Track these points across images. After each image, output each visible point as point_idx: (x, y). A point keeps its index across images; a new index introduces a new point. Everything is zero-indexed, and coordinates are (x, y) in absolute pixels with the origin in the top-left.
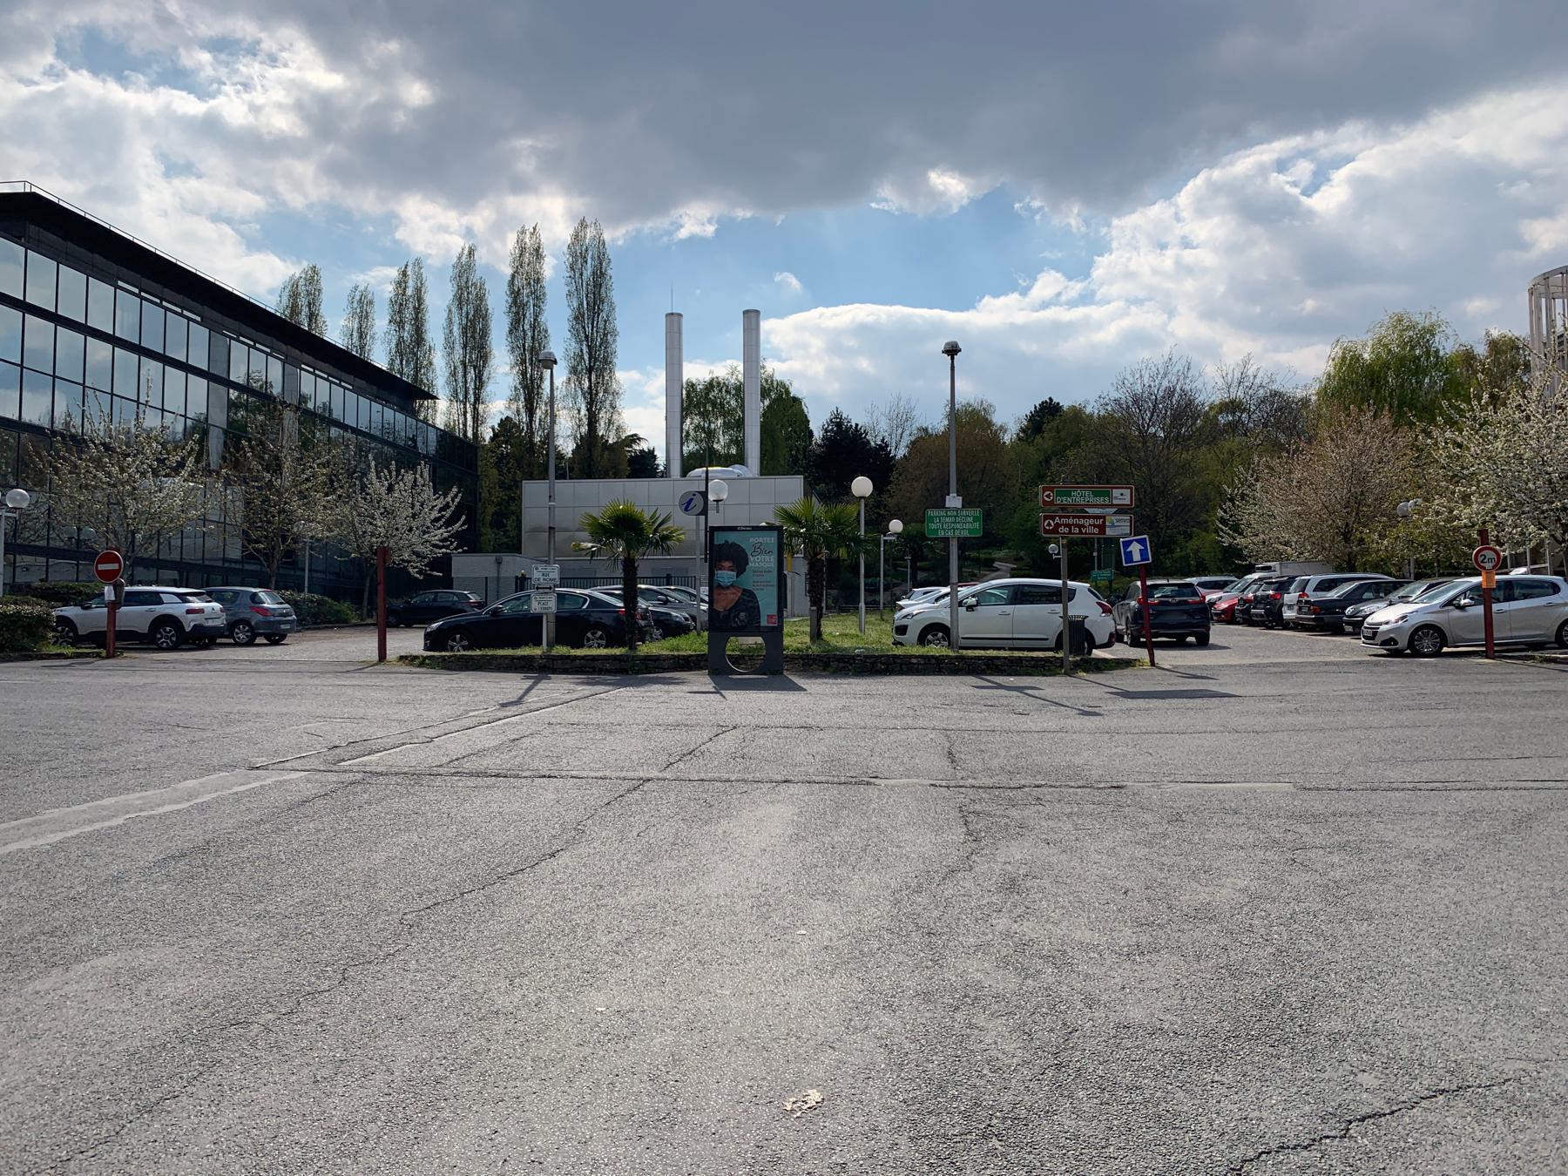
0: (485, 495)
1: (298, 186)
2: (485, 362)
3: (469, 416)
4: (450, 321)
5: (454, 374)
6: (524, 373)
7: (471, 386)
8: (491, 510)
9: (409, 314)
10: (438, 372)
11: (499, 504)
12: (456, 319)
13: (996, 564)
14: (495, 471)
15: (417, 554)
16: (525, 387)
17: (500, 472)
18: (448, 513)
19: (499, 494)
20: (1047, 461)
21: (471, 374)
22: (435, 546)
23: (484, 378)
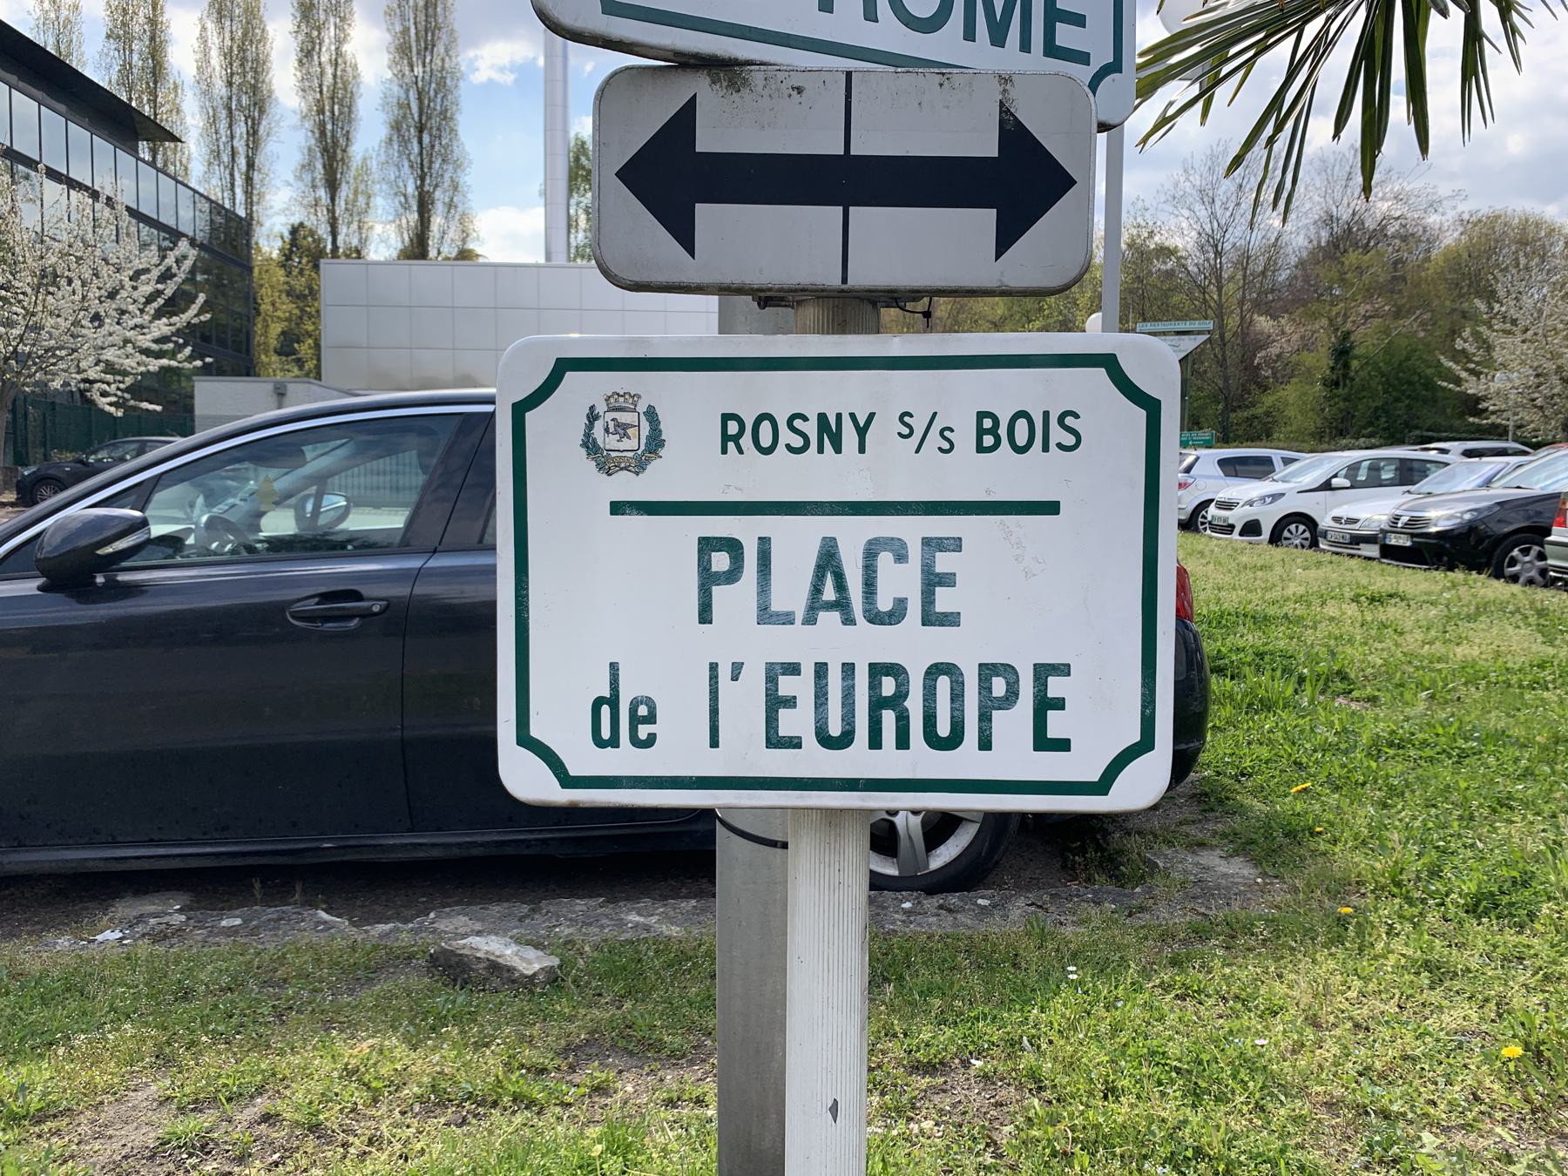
0: (265, 307)
1: (529, 962)
2: (262, 112)
3: (239, 191)
4: (203, 40)
5: (213, 121)
6: (323, 133)
7: (240, 145)
8: (276, 329)
9: (139, 25)
10: (189, 120)
11: (289, 320)
12: (214, 40)
13: (509, 78)
14: (282, 272)
15: (110, 368)
16: (325, 150)
17: (289, 274)
18: (170, 289)
19: (287, 307)
20: (1391, 596)
21: (241, 129)
22: (146, 352)
23: (262, 131)
